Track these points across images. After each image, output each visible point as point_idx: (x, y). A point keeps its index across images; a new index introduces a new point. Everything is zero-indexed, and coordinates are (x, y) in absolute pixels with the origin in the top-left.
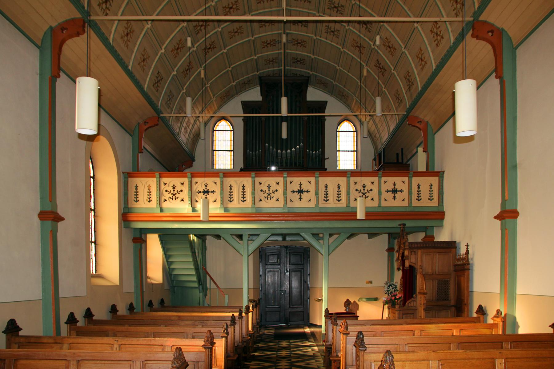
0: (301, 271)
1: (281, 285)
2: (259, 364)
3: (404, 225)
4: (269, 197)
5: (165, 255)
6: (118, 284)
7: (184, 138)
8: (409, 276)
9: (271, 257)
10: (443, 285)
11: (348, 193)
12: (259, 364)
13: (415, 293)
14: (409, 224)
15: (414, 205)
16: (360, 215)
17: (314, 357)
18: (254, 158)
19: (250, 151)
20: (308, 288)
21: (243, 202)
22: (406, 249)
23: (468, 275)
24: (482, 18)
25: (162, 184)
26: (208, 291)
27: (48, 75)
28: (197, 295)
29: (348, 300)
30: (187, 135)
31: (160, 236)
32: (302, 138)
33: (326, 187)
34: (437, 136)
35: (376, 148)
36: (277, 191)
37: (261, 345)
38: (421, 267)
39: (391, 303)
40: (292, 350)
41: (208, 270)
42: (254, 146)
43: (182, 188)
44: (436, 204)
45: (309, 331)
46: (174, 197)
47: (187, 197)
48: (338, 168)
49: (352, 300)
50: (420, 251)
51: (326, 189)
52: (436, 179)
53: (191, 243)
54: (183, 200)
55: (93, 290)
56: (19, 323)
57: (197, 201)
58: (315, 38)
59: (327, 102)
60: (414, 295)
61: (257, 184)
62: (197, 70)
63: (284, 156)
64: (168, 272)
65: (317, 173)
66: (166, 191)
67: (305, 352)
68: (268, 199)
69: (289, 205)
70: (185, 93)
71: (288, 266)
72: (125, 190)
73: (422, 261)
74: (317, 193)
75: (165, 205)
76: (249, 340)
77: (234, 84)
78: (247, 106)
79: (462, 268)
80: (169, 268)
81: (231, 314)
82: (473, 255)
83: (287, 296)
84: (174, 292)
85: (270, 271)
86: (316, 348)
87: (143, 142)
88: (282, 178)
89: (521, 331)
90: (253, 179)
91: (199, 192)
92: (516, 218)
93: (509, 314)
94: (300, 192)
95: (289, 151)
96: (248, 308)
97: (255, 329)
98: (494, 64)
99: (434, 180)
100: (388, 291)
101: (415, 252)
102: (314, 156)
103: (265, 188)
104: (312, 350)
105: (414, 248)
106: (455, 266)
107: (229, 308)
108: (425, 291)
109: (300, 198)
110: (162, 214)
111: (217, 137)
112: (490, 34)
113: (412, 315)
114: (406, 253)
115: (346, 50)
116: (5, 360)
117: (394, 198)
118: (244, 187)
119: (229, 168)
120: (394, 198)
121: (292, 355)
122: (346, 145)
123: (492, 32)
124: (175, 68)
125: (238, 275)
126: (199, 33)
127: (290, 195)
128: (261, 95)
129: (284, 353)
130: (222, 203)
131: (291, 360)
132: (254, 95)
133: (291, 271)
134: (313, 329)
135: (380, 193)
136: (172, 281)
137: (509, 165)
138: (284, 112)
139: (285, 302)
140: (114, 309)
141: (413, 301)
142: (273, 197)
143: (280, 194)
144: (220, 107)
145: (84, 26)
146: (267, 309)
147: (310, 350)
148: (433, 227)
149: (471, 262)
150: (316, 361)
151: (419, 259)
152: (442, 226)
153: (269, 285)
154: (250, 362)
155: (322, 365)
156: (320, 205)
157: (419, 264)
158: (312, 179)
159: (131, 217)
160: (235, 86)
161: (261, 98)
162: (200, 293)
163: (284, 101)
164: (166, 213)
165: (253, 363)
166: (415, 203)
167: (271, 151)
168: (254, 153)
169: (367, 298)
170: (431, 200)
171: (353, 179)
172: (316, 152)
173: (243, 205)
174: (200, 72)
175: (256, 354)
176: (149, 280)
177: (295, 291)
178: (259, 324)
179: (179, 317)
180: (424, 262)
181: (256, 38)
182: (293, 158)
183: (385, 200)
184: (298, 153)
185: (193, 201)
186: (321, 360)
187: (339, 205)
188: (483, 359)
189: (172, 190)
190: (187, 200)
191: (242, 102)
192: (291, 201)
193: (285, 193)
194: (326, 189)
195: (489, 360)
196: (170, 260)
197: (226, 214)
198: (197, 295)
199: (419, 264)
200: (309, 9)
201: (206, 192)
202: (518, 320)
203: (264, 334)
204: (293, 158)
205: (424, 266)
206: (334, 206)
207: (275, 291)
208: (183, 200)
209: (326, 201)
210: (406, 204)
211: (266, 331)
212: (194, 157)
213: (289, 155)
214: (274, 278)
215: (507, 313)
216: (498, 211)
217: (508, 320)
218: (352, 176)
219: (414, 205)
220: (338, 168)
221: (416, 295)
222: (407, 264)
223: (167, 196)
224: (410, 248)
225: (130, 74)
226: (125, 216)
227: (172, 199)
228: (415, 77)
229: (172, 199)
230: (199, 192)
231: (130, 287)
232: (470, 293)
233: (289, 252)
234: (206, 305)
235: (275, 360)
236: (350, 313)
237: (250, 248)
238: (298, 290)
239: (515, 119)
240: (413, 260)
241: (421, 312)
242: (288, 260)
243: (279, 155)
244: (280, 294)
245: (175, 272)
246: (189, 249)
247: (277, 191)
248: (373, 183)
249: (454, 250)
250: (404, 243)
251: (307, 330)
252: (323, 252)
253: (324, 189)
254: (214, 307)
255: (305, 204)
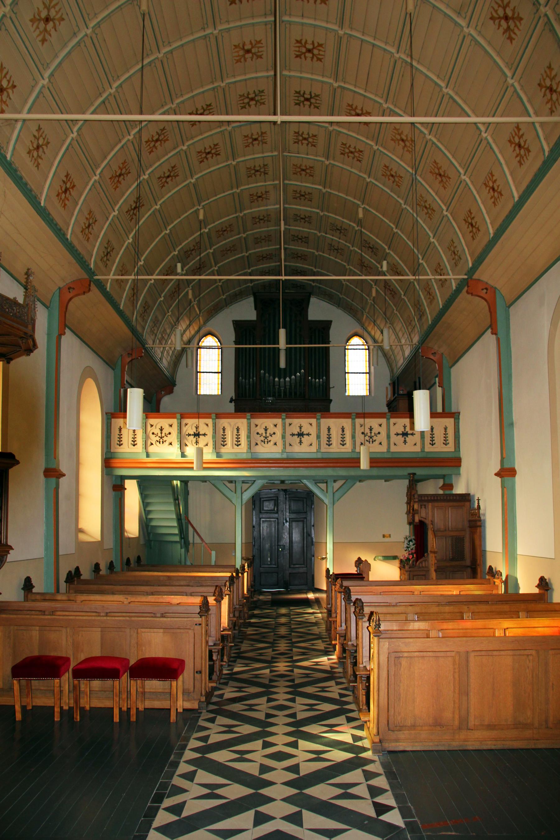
0: (303, 521)
1: (279, 538)
2: (256, 630)
3: (414, 474)
4: (266, 440)
5: (143, 502)
6: (100, 539)
7: (165, 364)
8: (420, 531)
9: (266, 504)
10: (458, 542)
11: (353, 437)
12: (256, 630)
13: (427, 552)
14: (420, 472)
15: (427, 450)
16: (364, 464)
17: (316, 624)
18: (247, 387)
19: (242, 379)
20: (312, 543)
21: (238, 446)
22: (415, 502)
23: (480, 532)
24: (475, 276)
25: (149, 426)
26: (191, 547)
27: (56, 333)
28: (179, 551)
29: (359, 558)
30: (169, 357)
31: (138, 482)
32: (302, 363)
33: (329, 429)
34: (453, 370)
35: (392, 371)
36: (274, 433)
37: (256, 612)
38: (432, 522)
39: (403, 565)
40: (292, 617)
41: (191, 519)
42: (248, 373)
43: (170, 430)
44: (452, 449)
45: (313, 598)
46: (162, 440)
47: (176, 440)
48: (347, 394)
49: (363, 559)
50: (430, 504)
51: (329, 432)
52: (452, 420)
53: (173, 488)
54: (171, 444)
55: (82, 546)
56: (34, 582)
57: (186, 445)
58: (324, 191)
59: (330, 322)
60: (426, 554)
61: (253, 426)
62: (184, 290)
63: (282, 384)
64: (145, 523)
65: (319, 415)
66: (153, 433)
67: (307, 619)
68: (264, 442)
69: (289, 449)
70: (163, 301)
71: (288, 514)
72: (107, 432)
73: (433, 516)
74: (318, 437)
75: (151, 449)
76: (244, 603)
77: (224, 297)
78: (239, 326)
79: (475, 524)
80: (146, 518)
81: (229, 574)
82: (485, 510)
83: (287, 552)
84: (151, 548)
85: (266, 521)
86: (320, 615)
87: (126, 375)
88: (280, 420)
89: (521, 592)
90: (249, 421)
91: (189, 435)
92: (515, 476)
93: (510, 576)
94: (301, 435)
95: (288, 379)
96: (243, 567)
97: (250, 592)
98: (489, 320)
99: (449, 422)
100: (407, 547)
101: (425, 505)
102: (317, 384)
103: (262, 431)
104: (315, 617)
105: (425, 501)
106: (470, 521)
107: (218, 567)
108: (436, 550)
109: (301, 442)
110: (148, 460)
111: (202, 356)
112: (485, 291)
113: (424, 577)
114: (416, 506)
115: (351, 267)
116: (44, 612)
117: (405, 442)
118: (238, 429)
119: (216, 394)
120: (405, 442)
121: (292, 622)
122: (357, 370)
123: (487, 289)
124: (162, 293)
125: (230, 528)
126: (189, 256)
127: (289, 438)
128: (256, 309)
129: (283, 620)
130: (215, 447)
131: (291, 640)
132: (246, 310)
133: (291, 521)
134: (317, 595)
135: (388, 437)
136: (149, 534)
137: (505, 424)
138: (282, 344)
139: (284, 561)
140: (97, 567)
141: (425, 561)
142: (270, 441)
143: (277, 438)
144: (206, 321)
145: (90, 285)
146: (262, 570)
147: (313, 617)
148: (451, 475)
149: (482, 518)
150: (318, 628)
151: (430, 513)
152: (460, 474)
153: (263, 539)
154: (247, 628)
155: (325, 631)
156: (323, 450)
157: (430, 518)
158: (313, 421)
159: (115, 463)
160: (225, 299)
161: (255, 313)
162: (181, 548)
163: (282, 333)
164: (153, 459)
165: (250, 629)
166: (428, 448)
167: (267, 378)
168: (247, 381)
169: (383, 556)
170: (446, 445)
171: (359, 421)
172: (319, 380)
173: (237, 450)
174: (187, 292)
175: (252, 621)
176: (126, 534)
177: (297, 547)
178: (254, 588)
179: (168, 577)
180: (437, 517)
181: (250, 254)
182: (293, 387)
183: (395, 444)
184: (298, 381)
185: (182, 445)
186: (324, 626)
187: (343, 449)
188: (453, 613)
189: (159, 432)
190: (176, 445)
191: (233, 321)
192: (290, 445)
193: (283, 437)
194: (329, 432)
195: (458, 614)
196: (149, 508)
197: (219, 460)
198: (179, 551)
199: (430, 518)
200: (309, 229)
201: (197, 435)
202: (519, 582)
203: (259, 600)
204: (293, 387)
205: (436, 521)
206: (338, 450)
207: (271, 547)
208: (171, 444)
209: (329, 445)
210: (418, 449)
211: (261, 597)
212: (175, 381)
213: (288, 384)
214: (271, 530)
215: (509, 574)
216: (497, 468)
217: (510, 582)
218: (357, 417)
219: (427, 450)
220: (347, 394)
221: (428, 555)
222: (417, 519)
223: (153, 439)
224: (420, 501)
225: (121, 313)
226: (108, 462)
227: (160, 442)
228: (425, 309)
229: (160, 442)
230: (189, 435)
231: (110, 544)
232: (484, 552)
233: (289, 501)
234: (188, 563)
235: (273, 627)
236: (361, 574)
237: (244, 497)
238: (300, 545)
239: (510, 376)
240: (423, 514)
241: (433, 575)
242: (288, 507)
243: (276, 384)
244: (278, 550)
245: (154, 523)
246: (171, 496)
247: (274, 433)
248: (380, 425)
249: (468, 503)
250: (414, 496)
251: (311, 596)
252: (326, 501)
253: (326, 432)
254: (195, 566)
255: (306, 449)
